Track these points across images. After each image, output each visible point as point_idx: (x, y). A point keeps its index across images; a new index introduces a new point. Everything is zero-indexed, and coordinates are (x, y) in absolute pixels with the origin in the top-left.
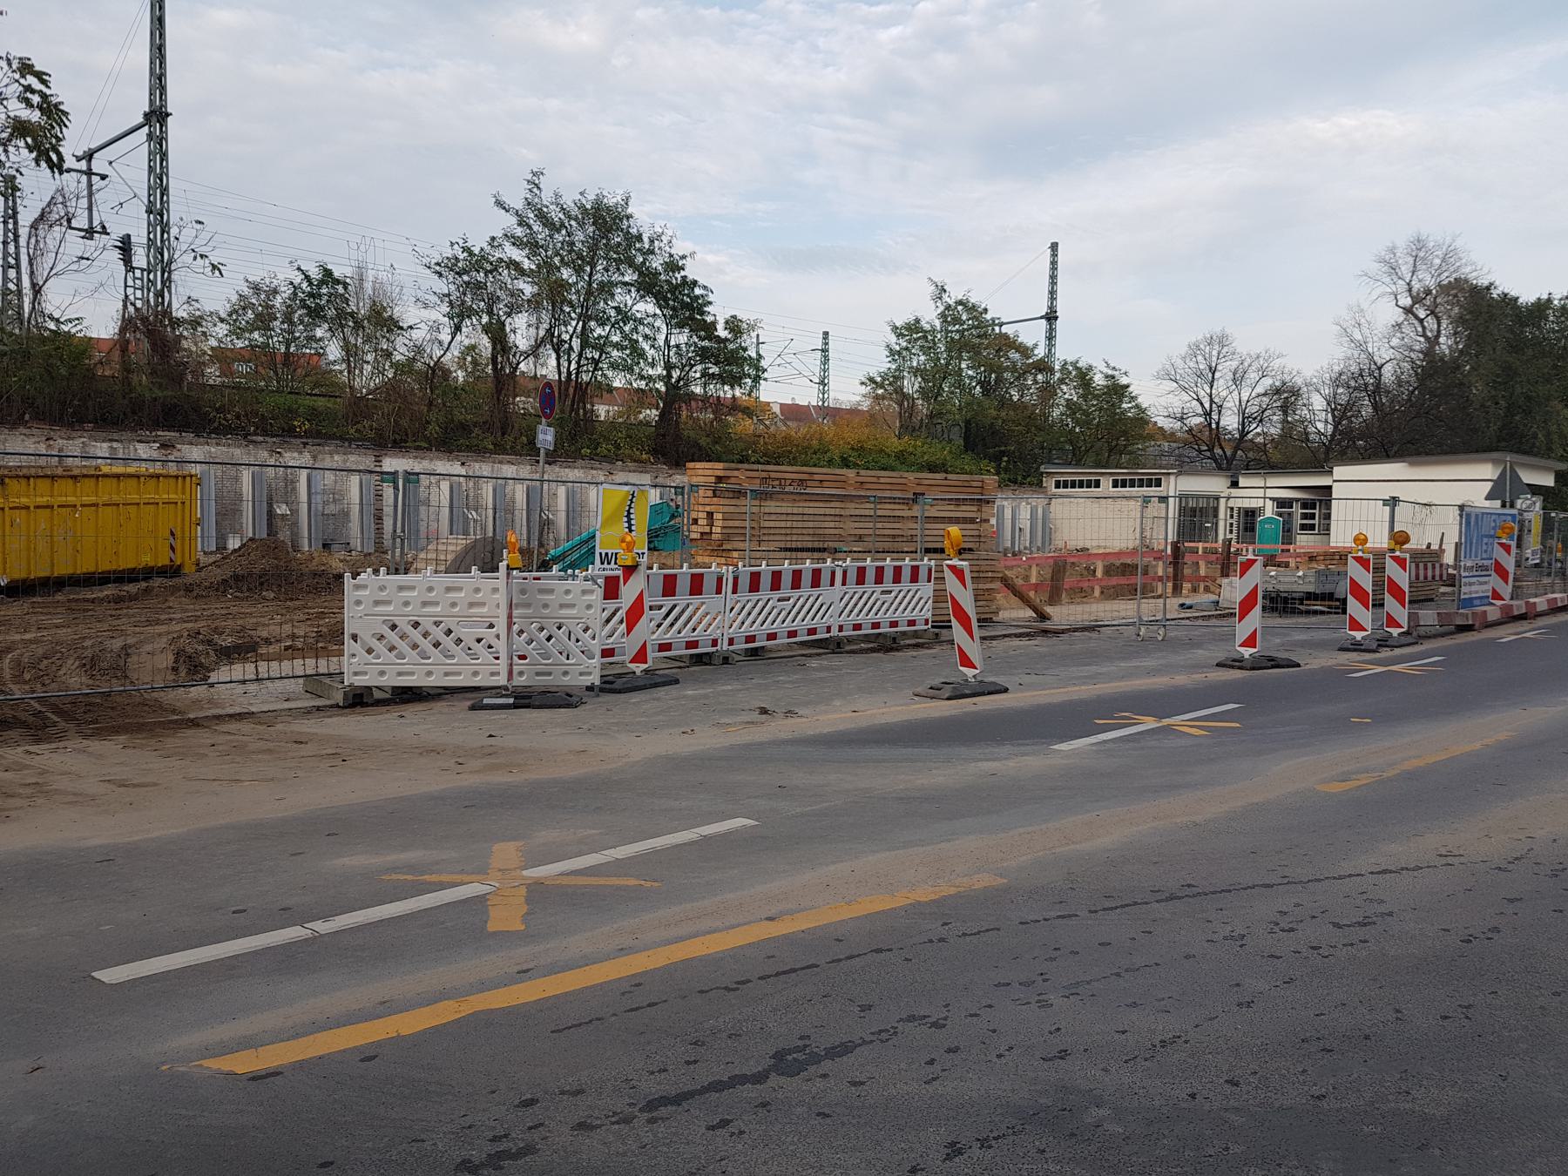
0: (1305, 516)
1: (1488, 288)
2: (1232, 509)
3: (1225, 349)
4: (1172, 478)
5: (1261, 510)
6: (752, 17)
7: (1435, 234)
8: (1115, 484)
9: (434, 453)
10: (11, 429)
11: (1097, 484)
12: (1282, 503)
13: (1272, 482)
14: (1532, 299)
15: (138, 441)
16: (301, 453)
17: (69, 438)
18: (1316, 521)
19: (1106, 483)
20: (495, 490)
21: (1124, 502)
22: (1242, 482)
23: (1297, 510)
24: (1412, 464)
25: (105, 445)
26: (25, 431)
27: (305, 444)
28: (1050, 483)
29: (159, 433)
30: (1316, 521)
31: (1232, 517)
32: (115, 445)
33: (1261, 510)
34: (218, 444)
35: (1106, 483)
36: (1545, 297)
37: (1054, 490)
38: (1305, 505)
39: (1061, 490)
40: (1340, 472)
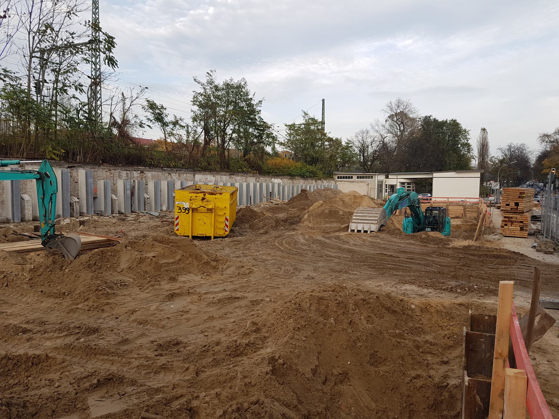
0: (408, 187)
1: (429, 117)
2: (386, 185)
3: (368, 135)
4: (376, 176)
5: (396, 185)
6: (130, 9)
7: (404, 99)
8: (358, 178)
9: (207, 173)
10: (99, 167)
11: (352, 178)
12: (403, 183)
13: (399, 177)
14: (441, 120)
15: (134, 171)
16: (176, 174)
17: (115, 170)
18: (411, 188)
19: (355, 177)
20: (62, 174)
21: (361, 183)
22: (390, 177)
23: (406, 185)
24: (457, 173)
25: (125, 172)
26: (103, 167)
27: (177, 170)
28: (336, 177)
29: (140, 167)
30: (411, 188)
31: (386, 187)
32: (128, 172)
33: (396, 185)
34: (155, 171)
35: (355, 177)
36: (445, 120)
37: (337, 179)
38: (408, 184)
39: (340, 179)
40: (435, 175)
